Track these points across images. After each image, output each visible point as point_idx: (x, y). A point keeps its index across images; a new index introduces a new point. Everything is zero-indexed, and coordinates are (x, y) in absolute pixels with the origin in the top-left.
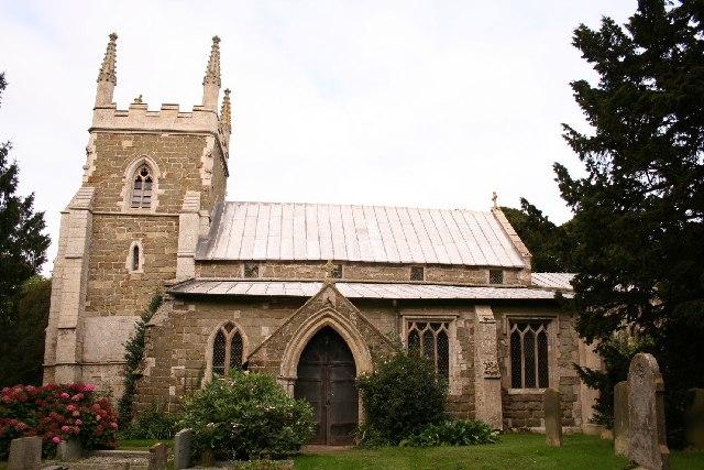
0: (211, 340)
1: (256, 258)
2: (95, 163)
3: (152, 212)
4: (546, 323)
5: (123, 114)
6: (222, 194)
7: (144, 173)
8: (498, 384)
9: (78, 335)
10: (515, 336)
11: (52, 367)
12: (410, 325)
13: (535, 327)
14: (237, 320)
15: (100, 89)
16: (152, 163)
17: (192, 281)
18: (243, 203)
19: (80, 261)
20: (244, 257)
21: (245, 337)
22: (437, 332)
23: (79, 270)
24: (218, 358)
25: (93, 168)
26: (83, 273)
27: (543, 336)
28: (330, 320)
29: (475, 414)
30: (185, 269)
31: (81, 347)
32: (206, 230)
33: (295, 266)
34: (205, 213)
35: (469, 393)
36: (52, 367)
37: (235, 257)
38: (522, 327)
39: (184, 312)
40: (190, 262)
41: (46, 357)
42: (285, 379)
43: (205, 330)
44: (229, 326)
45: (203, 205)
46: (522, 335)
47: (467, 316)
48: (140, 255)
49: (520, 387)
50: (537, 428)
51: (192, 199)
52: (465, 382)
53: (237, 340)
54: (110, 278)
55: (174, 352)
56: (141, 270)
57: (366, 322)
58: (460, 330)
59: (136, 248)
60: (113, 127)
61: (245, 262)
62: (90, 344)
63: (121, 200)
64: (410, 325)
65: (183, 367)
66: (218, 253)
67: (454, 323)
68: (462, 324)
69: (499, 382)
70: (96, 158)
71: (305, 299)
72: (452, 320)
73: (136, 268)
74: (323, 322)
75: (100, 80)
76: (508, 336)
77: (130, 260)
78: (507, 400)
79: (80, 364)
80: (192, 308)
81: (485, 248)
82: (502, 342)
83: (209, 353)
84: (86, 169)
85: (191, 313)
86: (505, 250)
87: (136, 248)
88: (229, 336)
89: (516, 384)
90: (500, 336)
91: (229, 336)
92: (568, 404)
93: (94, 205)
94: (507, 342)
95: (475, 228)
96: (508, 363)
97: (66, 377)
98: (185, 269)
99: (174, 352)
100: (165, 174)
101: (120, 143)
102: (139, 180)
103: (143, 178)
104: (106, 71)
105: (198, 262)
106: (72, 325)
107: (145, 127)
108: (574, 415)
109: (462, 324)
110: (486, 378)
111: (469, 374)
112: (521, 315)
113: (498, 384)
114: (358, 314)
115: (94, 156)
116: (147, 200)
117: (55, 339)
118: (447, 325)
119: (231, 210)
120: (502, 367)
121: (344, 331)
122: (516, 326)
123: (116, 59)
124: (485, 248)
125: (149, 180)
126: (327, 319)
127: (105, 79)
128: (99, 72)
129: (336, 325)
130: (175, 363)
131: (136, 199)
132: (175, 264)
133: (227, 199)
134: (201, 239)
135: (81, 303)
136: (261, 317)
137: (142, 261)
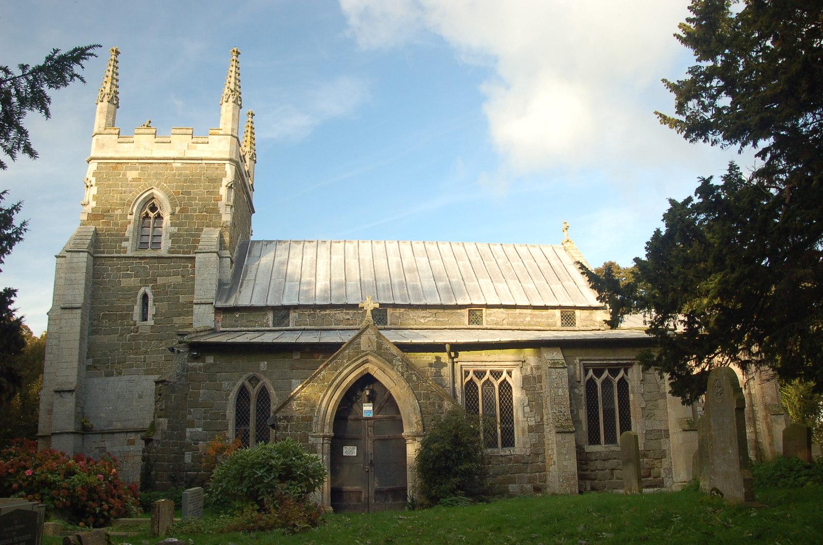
0: (232, 396)
1: (286, 302)
3: (163, 251)
4: (627, 367)
6: (247, 232)
8: (571, 438)
9: (77, 398)
10: (591, 385)
11: (47, 438)
12: (586, 372)
13: (614, 372)
14: (264, 373)
17: (213, 331)
18: (271, 242)
19: (79, 311)
20: (271, 302)
21: (272, 392)
22: (617, 379)
23: (78, 322)
24: (242, 418)
26: (82, 325)
27: (623, 384)
29: (545, 475)
31: (81, 414)
32: (229, 273)
33: (332, 312)
35: (538, 450)
36: (47, 438)
37: (261, 304)
38: (598, 372)
39: (201, 364)
40: (210, 310)
43: (225, 384)
44: (254, 380)
46: (599, 382)
48: (150, 303)
49: (598, 443)
50: (100, 250)
52: (534, 437)
53: (264, 395)
54: (114, 332)
55: (190, 413)
56: (151, 322)
59: (145, 296)
61: (274, 309)
63: (127, 240)
65: (200, 429)
66: (244, 298)
69: (573, 436)
70: (95, 193)
71: (337, 346)
72: (631, 365)
73: (145, 318)
76: (582, 383)
77: (137, 309)
78: (583, 459)
79: (85, 430)
80: (210, 360)
81: (557, 287)
82: (576, 391)
83: (231, 413)
85: (207, 368)
87: (145, 296)
88: (253, 392)
89: (594, 440)
90: (573, 383)
91: (253, 392)
92: (656, 462)
93: (95, 247)
94: (582, 390)
95: (543, 264)
96: (583, 414)
98: (203, 317)
99: (190, 413)
100: (178, 209)
101: (124, 175)
103: (152, 215)
105: (218, 310)
106: (72, 387)
107: (155, 155)
108: (663, 475)
110: (557, 432)
111: (537, 429)
112: (598, 358)
113: (571, 438)
117: (52, 404)
119: (256, 251)
120: (576, 421)
121: (76, 305)
122: (591, 373)
124: (557, 287)
130: (191, 424)
132: (190, 313)
133: (252, 238)
134: (221, 284)
135: (80, 361)
136: (292, 368)
137: (151, 310)
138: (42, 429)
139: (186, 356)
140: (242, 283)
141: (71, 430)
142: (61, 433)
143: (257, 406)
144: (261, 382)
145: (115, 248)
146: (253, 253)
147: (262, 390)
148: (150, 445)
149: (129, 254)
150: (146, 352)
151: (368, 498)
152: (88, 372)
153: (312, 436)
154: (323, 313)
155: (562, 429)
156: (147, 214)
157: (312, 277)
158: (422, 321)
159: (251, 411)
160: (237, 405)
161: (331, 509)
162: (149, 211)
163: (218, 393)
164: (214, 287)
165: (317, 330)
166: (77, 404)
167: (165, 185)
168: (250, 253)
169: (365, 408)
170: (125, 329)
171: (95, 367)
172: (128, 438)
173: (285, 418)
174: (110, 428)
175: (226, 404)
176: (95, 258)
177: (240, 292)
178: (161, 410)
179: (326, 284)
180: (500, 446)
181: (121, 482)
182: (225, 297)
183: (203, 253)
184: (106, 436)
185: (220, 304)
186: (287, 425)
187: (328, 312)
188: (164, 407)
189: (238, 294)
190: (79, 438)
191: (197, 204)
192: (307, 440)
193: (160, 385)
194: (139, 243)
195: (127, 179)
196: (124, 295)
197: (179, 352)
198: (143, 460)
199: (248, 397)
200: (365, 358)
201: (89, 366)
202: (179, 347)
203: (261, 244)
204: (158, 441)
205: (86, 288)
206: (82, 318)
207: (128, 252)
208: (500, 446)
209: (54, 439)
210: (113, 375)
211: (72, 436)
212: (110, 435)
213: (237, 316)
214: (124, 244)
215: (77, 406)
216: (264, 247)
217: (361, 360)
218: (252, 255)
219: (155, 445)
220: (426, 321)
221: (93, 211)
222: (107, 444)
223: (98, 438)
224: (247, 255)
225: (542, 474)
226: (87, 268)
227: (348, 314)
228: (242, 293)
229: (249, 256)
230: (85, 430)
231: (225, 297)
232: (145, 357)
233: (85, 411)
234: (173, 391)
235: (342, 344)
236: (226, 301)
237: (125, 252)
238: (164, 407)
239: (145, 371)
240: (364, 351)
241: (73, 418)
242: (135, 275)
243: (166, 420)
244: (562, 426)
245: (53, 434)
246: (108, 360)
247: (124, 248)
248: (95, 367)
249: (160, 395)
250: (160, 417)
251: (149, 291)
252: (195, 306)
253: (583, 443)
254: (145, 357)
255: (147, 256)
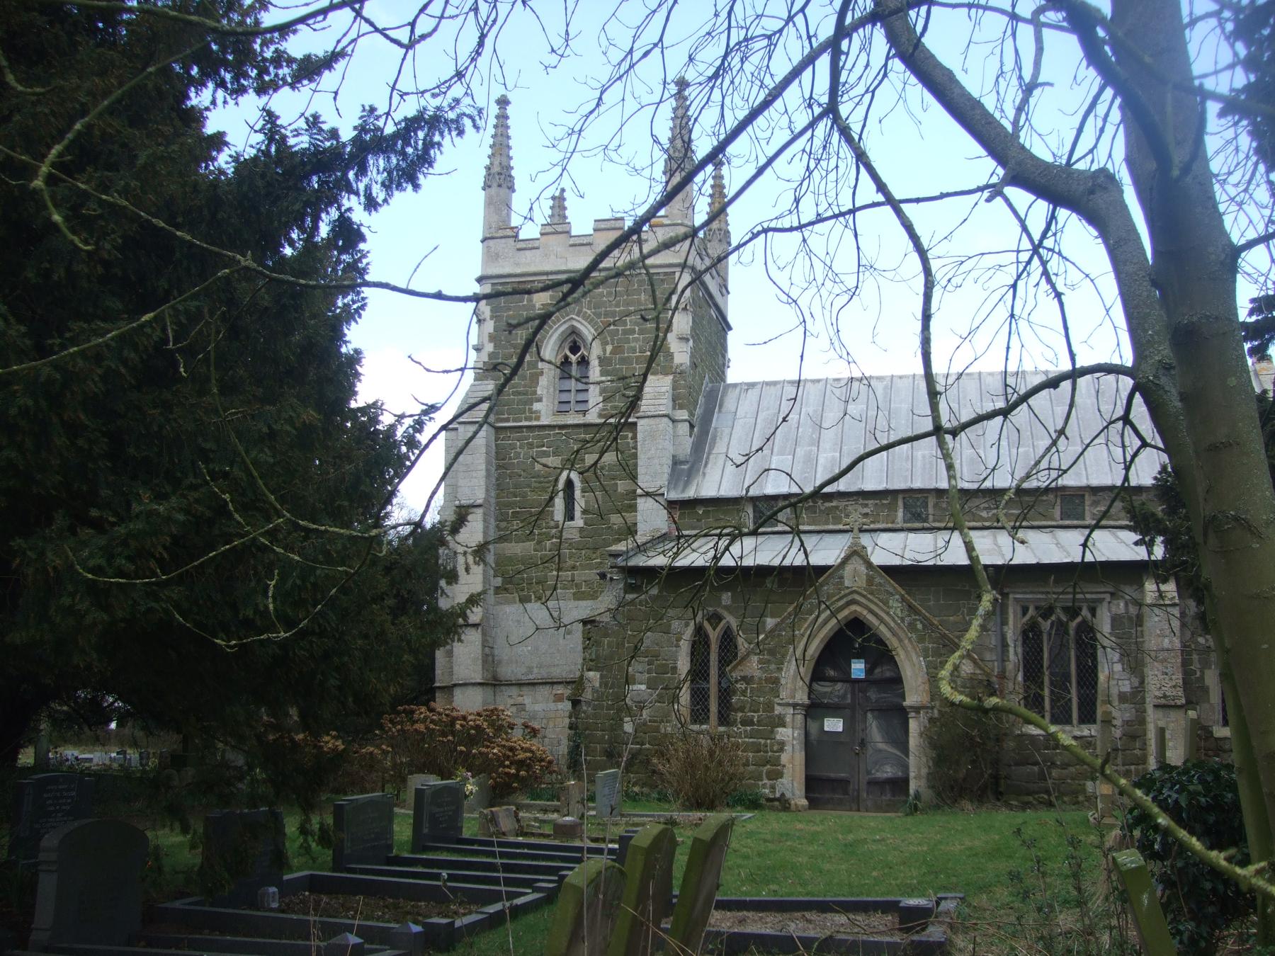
2: (492, 338)
5: (530, 246)
7: (575, 349)
9: (484, 634)
11: (449, 689)
15: (489, 203)
16: (587, 331)
25: (489, 347)
28: (858, 609)
30: (651, 517)
34: (683, 414)
36: (449, 689)
41: (438, 672)
42: (788, 705)
45: (677, 402)
47: (1129, 591)
48: (578, 493)
51: (658, 389)
56: (579, 522)
57: (917, 612)
58: (1116, 620)
59: (569, 483)
60: (518, 271)
61: (754, 500)
62: (503, 652)
63: (540, 400)
64: (1025, 611)
65: (643, 687)
67: (1105, 604)
68: (1120, 607)
72: (1101, 601)
73: (570, 515)
74: (846, 612)
75: (486, 187)
79: (494, 683)
84: (478, 349)
86: (1154, 482)
87: (569, 483)
88: (714, 635)
91: (714, 635)
97: (469, 702)
100: (609, 348)
102: (566, 362)
104: (496, 169)
105: (671, 505)
106: (479, 502)
109: (1120, 607)
114: (903, 599)
115: (490, 326)
116: (581, 397)
118: (1093, 611)
119: (730, 402)
123: (511, 153)
125: (584, 362)
126: (854, 608)
127: (495, 185)
128: (484, 172)
129: (865, 612)
131: (565, 397)
132: (633, 508)
133: (732, 376)
134: (676, 462)
138: (440, 679)
139: (621, 585)
140: (708, 458)
141: (479, 681)
142: (465, 685)
143: (719, 655)
144: (724, 622)
145: (524, 412)
146: (726, 404)
147: (725, 632)
148: (577, 708)
149: (545, 421)
150: (574, 568)
151: (858, 791)
152: (490, 731)
153: (779, 704)
154: (828, 504)
155: (1163, 701)
156: (566, 357)
157: (812, 445)
158: (984, 514)
159: (712, 663)
160: (692, 653)
161: (804, 802)
162: (568, 353)
163: (665, 636)
164: (667, 470)
165: (819, 532)
166: (485, 644)
167: (589, 312)
168: (721, 406)
169: (853, 666)
170: (545, 533)
171: (505, 589)
172: (554, 692)
173: (744, 679)
174: (531, 677)
175: (677, 652)
176: (497, 429)
177: (704, 474)
178: (591, 660)
179: (833, 457)
180: (1075, 721)
181: (1137, 684)
182: (681, 484)
183: (648, 417)
184: (525, 689)
185: (673, 496)
186: (746, 688)
187: (834, 504)
188: (594, 657)
189: (700, 478)
190: (489, 690)
191: (636, 340)
192: (773, 710)
193: (589, 626)
194: (556, 402)
195: (534, 306)
196: (540, 482)
197: (611, 579)
198: (570, 728)
199: (706, 643)
200: (850, 598)
201: (497, 588)
202: (611, 573)
203: (738, 390)
204: (588, 703)
205: (488, 476)
206: (485, 521)
207: (542, 418)
208: (1075, 721)
209: (458, 693)
210: (530, 601)
211: (479, 690)
212: (531, 688)
213: (701, 512)
214: (536, 406)
215: (484, 646)
216: (743, 396)
217: (845, 600)
218: (724, 410)
219: (585, 708)
220: (990, 514)
221: (490, 359)
222: (527, 700)
223: (514, 691)
224: (717, 410)
225: (1140, 767)
226: (487, 446)
227: (866, 505)
228: (707, 476)
229: (720, 411)
230: (494, 683)
231: (681, 488)
232: (573, 575)
233: (496, 652)
234: (606, 635)
235: (830, 567)
236: (683, 491)
237: (538, 418)
238: (594, 657)
239: (574, 594)
240: (848, 588)
241: (480, 662)
242: (554, 453)
243: (598, 675)
244: (1165, 696)
245: (455, 685)
246: (523, 579)
247: (536, 412)
248: (505, 589)
249: (589, 639)
250: (589, 670)
251: (574, 476)
252: (639, 500)
253: (1210, 724)
254: (573, 575)
255: (569, 423)
